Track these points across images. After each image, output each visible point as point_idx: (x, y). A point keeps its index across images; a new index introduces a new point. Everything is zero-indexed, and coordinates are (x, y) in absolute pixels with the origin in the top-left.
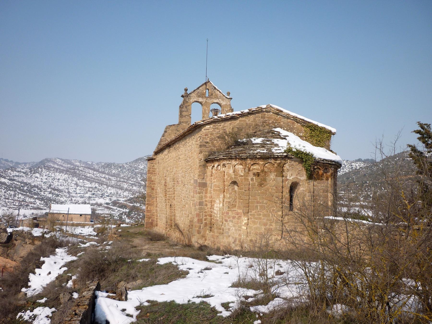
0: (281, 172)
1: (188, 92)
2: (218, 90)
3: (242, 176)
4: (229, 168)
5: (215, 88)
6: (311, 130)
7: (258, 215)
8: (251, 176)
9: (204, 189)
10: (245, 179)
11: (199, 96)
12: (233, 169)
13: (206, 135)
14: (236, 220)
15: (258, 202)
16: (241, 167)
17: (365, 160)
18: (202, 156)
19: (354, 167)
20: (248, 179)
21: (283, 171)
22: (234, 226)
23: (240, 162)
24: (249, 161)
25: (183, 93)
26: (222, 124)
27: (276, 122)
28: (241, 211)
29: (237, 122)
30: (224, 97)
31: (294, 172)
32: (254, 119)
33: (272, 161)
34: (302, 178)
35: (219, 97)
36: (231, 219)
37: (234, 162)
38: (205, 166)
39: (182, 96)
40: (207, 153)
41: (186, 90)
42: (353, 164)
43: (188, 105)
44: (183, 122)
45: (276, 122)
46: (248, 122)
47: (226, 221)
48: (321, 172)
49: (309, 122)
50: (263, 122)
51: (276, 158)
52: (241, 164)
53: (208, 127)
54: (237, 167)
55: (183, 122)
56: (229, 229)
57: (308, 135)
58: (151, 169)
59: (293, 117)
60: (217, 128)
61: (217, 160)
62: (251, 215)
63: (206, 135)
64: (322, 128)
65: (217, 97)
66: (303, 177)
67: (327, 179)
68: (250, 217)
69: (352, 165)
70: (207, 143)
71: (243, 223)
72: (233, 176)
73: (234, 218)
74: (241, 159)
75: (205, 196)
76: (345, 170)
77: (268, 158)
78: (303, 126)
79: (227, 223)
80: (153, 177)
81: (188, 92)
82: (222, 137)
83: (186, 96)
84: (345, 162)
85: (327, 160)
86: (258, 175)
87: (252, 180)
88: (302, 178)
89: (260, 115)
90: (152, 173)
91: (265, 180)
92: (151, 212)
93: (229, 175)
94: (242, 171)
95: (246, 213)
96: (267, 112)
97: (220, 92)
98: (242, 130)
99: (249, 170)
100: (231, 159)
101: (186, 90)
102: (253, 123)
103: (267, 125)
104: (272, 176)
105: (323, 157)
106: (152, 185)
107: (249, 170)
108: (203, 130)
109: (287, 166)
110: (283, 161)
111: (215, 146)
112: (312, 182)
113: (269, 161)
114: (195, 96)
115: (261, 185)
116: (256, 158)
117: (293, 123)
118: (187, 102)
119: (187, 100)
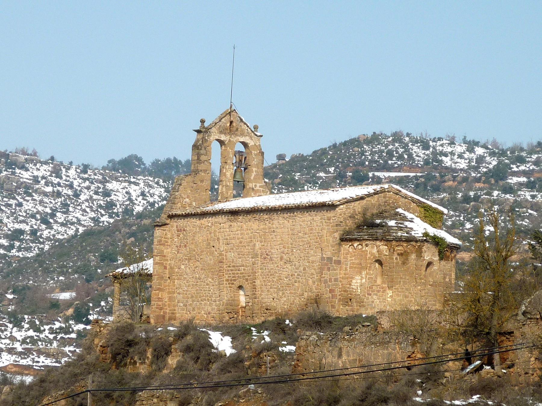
0: (419, 253)
1: (206, 125)
2: (245, 124)
3: (387, 255)
4: (373, 248)
5: (241, 120)
6: (425, 210)
7: (401, 289)
8: (395, 256)
9: (339, 266)
10: (389, 258)
11: (221, 132)
12: (375, 249)
13: (340, 215)
14: (381, 293)
15: (401, 278)
16: (386, 247)
17: (156, 163)
18: (337, 235)
19: (119, 197)
20: (393, 258)
21: (421, 252)
22: (378, 299)
23: (385, 243)
24: (394, 243)
25: (198, 127)
26: (353, 204)
27: (395, 202)
28: (386, 285)
29: (364, 202)
30: (253, 134)
31: (430, 253)
32: (378, 199)
33: (414, 243)
34: (435, 259)
35: (246, 134)
36: (376, 292)
37: (378, 243)
38: (340, 245)
39: (198, 132)
40: (342, 233)
41: (203, 121)
42: (112, 185)
43: (207, 145)
44: (201, 171)
45: (395, 202)
46: (373, 202)
47: (370, 295)
48: (448, 254)
49: (424, 203)
50: (385, 202)
51: (417, 241)
52: (386, 245)
53: (342, 206)
54: (381, 247)
55: (201, 171)
56: (373, 302)
57: (423, 215)
58: (163, 239)
59: (411, 197)
60: (349, 208)
61: (358, 240)
62: (395, 289)
63: (340, 215)
64: (436, 209)
65: (242, 134)
66: (437, 258)
67: (452, 261)
68: (394, 290)
69: (107, 193)
70: (341, 222)
71: (389, 296)
72: (377, 255)
73: (379, 291)
74: (387, 240)
75: (340, 273)
76: (75, 214)
77: (411, 241)
78: (418, 206)
79: (370, 297)
80: (165, 251)
81: (206, 125)
82: (352, 217)
83: (203, 131)
84: (72, 172)
85: (453, 244)
86: (401, 255)
87: (396, 259)
88: (435, 259)
89: (382, 195)
90: (164, 245)
91: (407, 259)
92: (162, 301)
93: (372, 254)
94: (386, 251)
95: (390, 288)
96: (388, 192)
97: (248, 126)
98: (368, 210)
99: (394, 251)
100: (377, 239)
101: (203, 121)
102: (377, 203)
103: (388, 205)
104: (413, 256)
105: (454, 242)
106: (164, 262)
107: (394, 251)
108: (337, 209)
109: (424, 249)
110: (422, 244)
111: (347, 226)
112: (443, 263)
113: (412, 243)
114: (216, 132)
115: (404, 263)
116: (402, 241)
117: (410, 203)
118: (206, 140)
119: (206, 138)
